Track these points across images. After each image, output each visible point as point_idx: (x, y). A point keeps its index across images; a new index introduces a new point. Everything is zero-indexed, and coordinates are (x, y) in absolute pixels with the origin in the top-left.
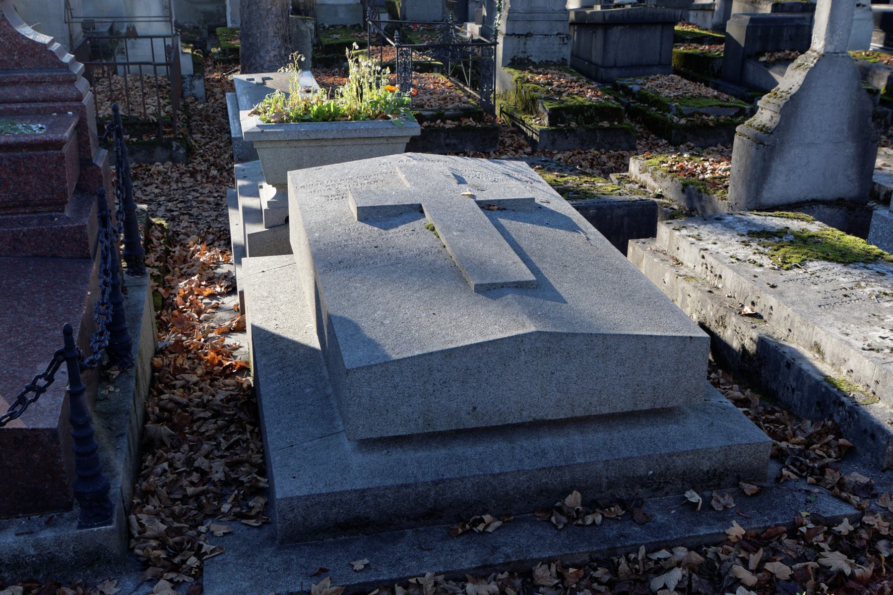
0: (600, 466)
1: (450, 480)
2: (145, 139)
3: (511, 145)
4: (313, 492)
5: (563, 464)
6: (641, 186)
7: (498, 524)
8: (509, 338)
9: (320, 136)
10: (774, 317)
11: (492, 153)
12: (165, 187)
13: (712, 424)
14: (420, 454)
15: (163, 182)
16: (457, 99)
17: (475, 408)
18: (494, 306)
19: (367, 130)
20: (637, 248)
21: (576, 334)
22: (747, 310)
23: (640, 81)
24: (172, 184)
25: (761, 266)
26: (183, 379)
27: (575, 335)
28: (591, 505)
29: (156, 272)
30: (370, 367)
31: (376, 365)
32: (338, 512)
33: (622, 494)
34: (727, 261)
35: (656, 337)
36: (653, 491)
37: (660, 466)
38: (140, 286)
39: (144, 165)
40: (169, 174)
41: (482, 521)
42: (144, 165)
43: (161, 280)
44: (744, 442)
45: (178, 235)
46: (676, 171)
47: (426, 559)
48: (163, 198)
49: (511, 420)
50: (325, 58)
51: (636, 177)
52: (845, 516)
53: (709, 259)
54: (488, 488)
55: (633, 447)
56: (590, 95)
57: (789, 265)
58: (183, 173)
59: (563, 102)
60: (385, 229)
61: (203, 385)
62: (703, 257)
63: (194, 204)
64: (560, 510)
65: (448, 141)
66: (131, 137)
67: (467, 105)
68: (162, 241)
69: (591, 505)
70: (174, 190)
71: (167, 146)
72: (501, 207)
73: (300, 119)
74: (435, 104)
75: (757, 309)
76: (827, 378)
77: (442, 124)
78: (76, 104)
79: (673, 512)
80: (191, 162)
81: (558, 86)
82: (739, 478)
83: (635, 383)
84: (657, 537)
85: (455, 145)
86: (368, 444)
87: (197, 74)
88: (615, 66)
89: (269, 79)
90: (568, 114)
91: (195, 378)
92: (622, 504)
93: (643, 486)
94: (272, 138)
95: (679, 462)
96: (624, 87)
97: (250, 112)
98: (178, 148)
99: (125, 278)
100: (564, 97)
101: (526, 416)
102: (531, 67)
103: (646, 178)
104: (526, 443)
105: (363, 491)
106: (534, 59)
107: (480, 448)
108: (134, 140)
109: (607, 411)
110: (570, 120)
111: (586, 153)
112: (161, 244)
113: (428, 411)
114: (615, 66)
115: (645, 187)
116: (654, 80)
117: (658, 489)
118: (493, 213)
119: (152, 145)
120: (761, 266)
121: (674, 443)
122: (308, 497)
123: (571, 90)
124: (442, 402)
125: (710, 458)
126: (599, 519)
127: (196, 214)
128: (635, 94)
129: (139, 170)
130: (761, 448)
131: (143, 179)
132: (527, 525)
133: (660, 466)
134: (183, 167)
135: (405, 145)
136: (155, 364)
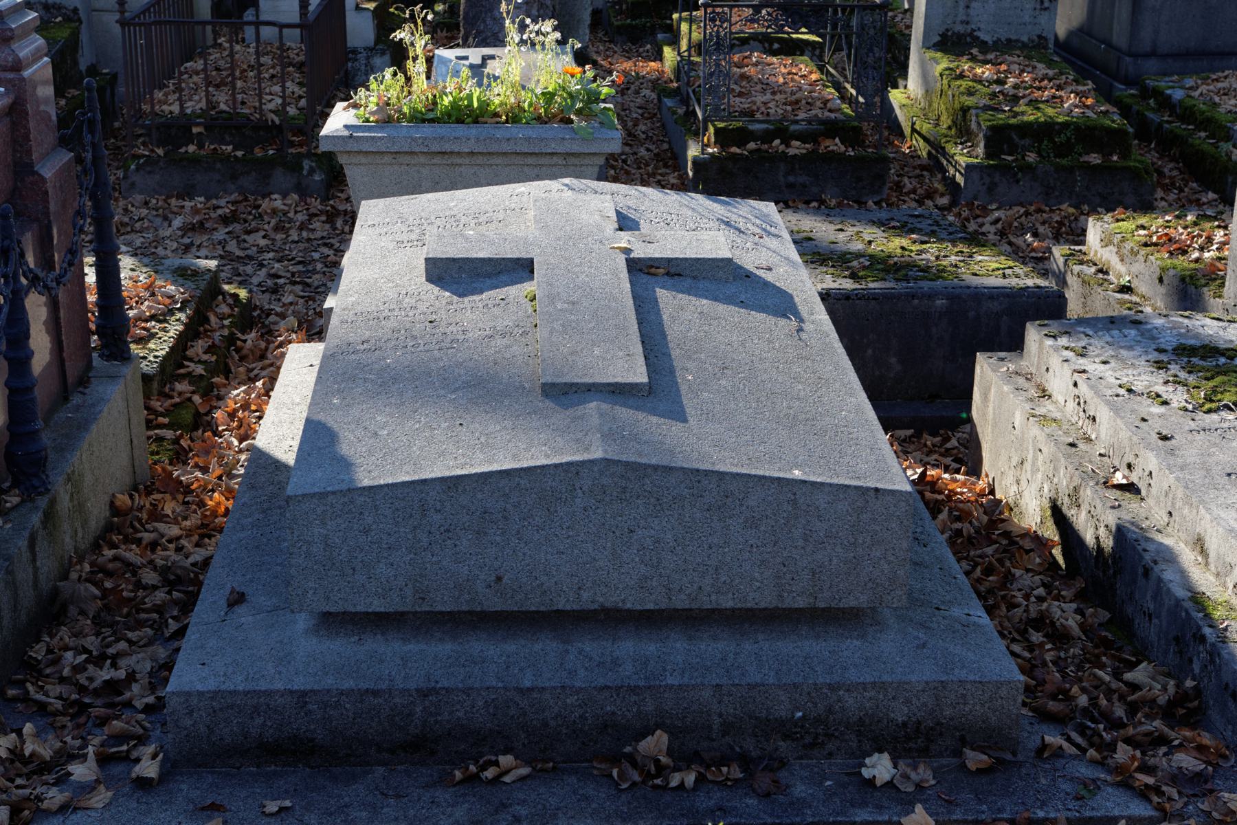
0: (707, 694)
1: (447, 690)
2: (258, 152)
3: (914, 191)
4: (223, 687)
5: (642, 683)
6: (1100, 271)
7: (524, 771)
8: (556, 466)
9: (447, 147)
10: (1154, 490)
11: (870, 203)
12: (279, 236)
13: (924, 645)
14: (411, 646)
15: (277, 229)
16: (818, 104)
17: (499, 579)
18: (561, 417)
19: (528, 139)
20: (986, 365)
21: (671, 468)
22: (1119, 478)
23: (1190, 82)
24: (292, 232)
25: (1165, 403)
26: (155, 530)
27: (668, 469)
28: (682, 757)
29: (199, 370)
30: (323, 495)
31: (333, 493)
32: (264, 724)
33: (749, 745)
34: (1109, 392)
35: (813, 484)
36: (804, 746)
37: (815, 704)
38: (113, 377)
39: (251, 198)
40: (291, 215)
41: (496, 763)
42: (251, 198)
43: (204, 384)
44: (972, 677)
45: (268, 315)
46: (1156, 244)
47: (385, 810)
48: (271, 255)
49: (561, 604)
50: (630, 26)
51: (1096, 252)
52: (1122, 817)
53: (1083, 388)
54: (512, 712)
55: (773, 668)
56: (1070, 103)
57: (1213, 405)
58: (316, 215)
59: (1016, 115)
60: (460, 296)
61: (184, 542)
62: (1075, 385)
63: (319, 266)
64: (632, 760)
65: (791, 179)
66: (235, 149)
67: (833, 116)
68: (226, 322)
69: (682, 757)
70: (293, 242)
71: (294, 166)
72: (673, 271)
73: (418, 118)
74: (775, 111)
75: (1134, 478)
76: (1198, 600)
77: (782, 148)
78: (10, 75)
79: (828, 783)
80: (334, 197)
81: (1016, 87)
82: (963, 741)
83: (779, 560)
84: (778, 817)
85: (804, 186)
86: (334, 622)
87: (380, 47)
88: (1153, 54)
89: (492, 57)
90: (1022, 137)
91: (175, 531)
92: (745, 761)
93: (786, 737)
94: (366, 147)
95: (850, 701)
96: (1157, 93)
97: (346, 104)
98: (312, 171)
99: (95, 363)
100: (1021, 107)
101: (588, 599)
102: (975, 51)
103: (1108, 256)
104: (590, 646)
105: (304, 694)
106: (983, 36)
107: (511, 647)
108: (239, 154)
109: (730, 604)
110: (1026, 149)
111: (1052, 211)
112: (223, 327)
113: (421, 575)
114: (1153, 54)
115: (1107, 273)
116: (1217, 80)
117: (812, 745)
118: (654, 279)
119: (265, 167)
120: (1165, 403)
121: (845, 669)
122: (216, 694)
123: (1037, 94)
124: (444, 563)
125: (908, 701)
126: (690, 779)
127: (316, 283)
128: (1174, 106)
129: (241, 208)
130: (1003, 692)
131: (245, 221)
132: (573, 779)
133: (815, 704)
134: (316, 204)
135: (596, 169)
136: (118, 503)
